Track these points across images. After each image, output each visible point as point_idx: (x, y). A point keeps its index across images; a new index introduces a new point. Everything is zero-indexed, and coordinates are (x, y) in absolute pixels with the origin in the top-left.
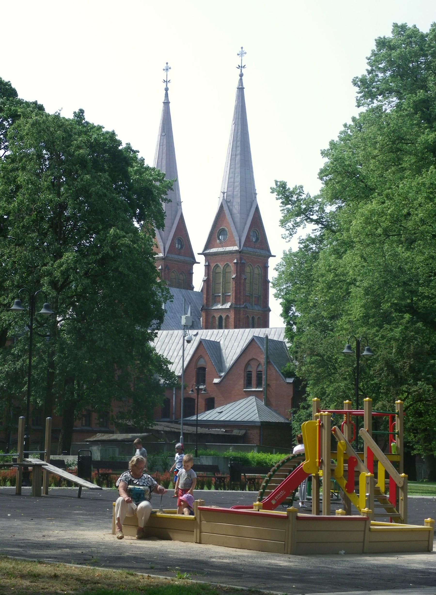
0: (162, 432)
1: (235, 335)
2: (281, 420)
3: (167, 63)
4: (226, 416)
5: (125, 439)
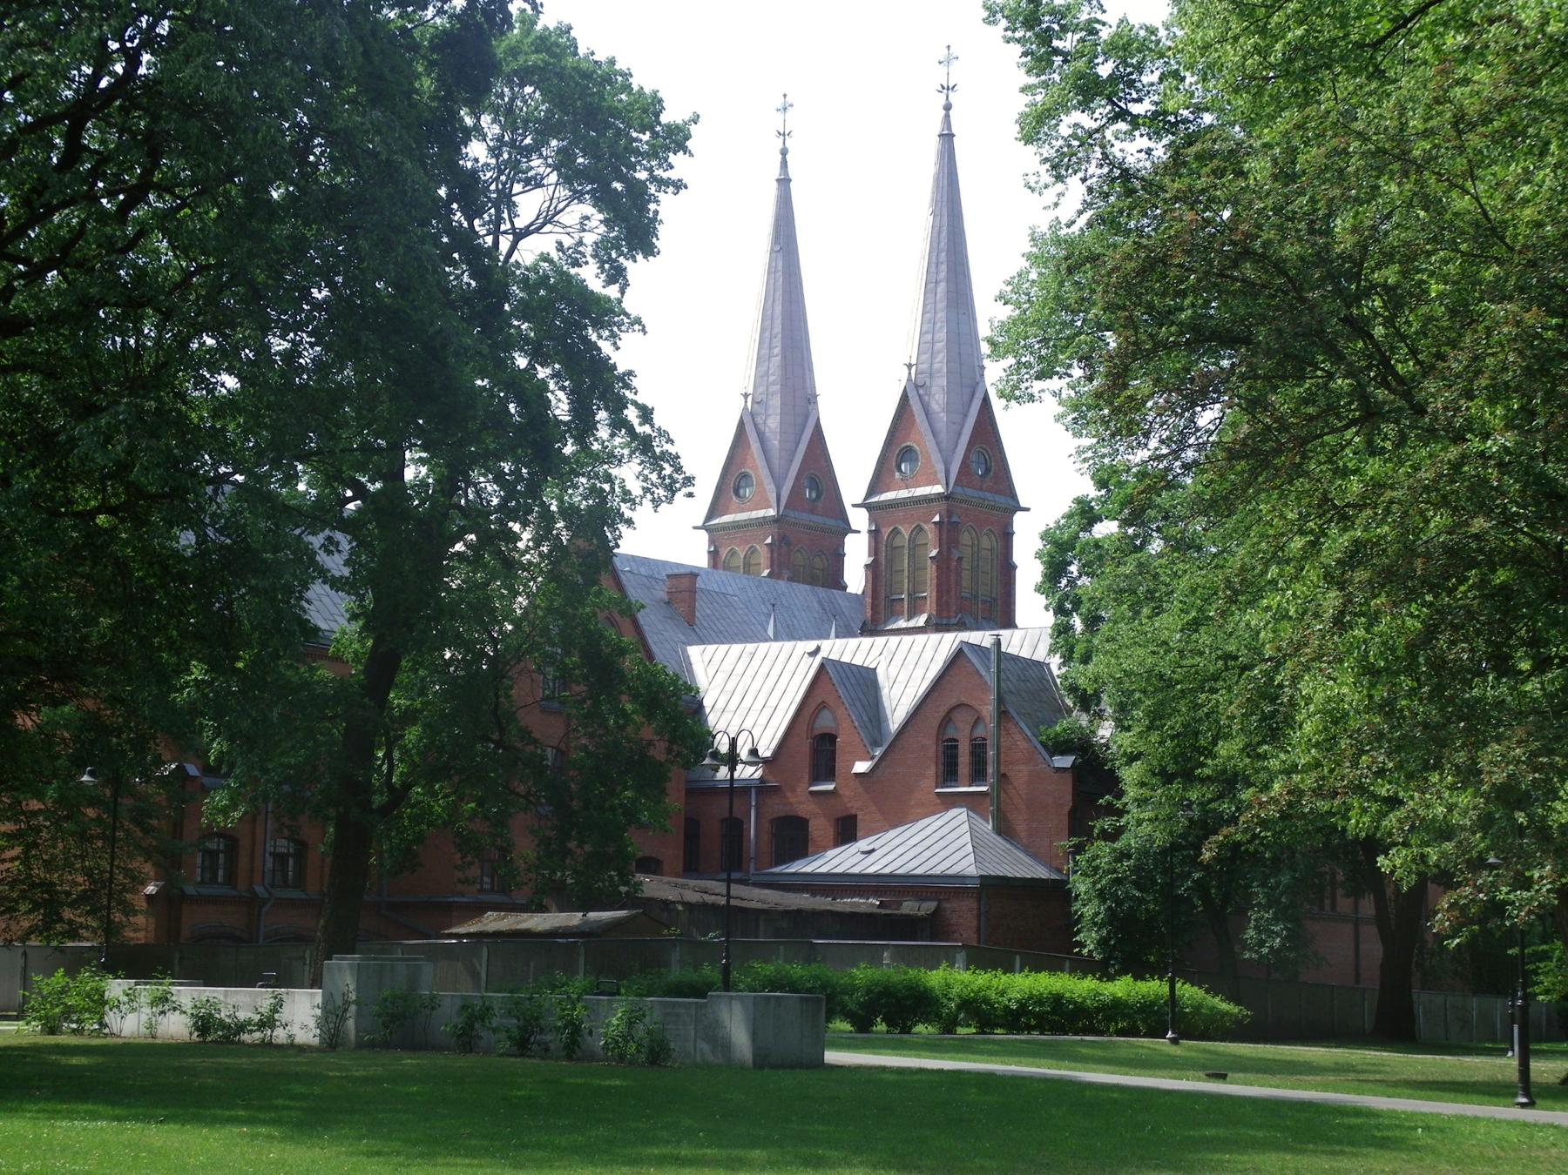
0: (680, 908)
1: (917, 649)
2: (1042, 872)
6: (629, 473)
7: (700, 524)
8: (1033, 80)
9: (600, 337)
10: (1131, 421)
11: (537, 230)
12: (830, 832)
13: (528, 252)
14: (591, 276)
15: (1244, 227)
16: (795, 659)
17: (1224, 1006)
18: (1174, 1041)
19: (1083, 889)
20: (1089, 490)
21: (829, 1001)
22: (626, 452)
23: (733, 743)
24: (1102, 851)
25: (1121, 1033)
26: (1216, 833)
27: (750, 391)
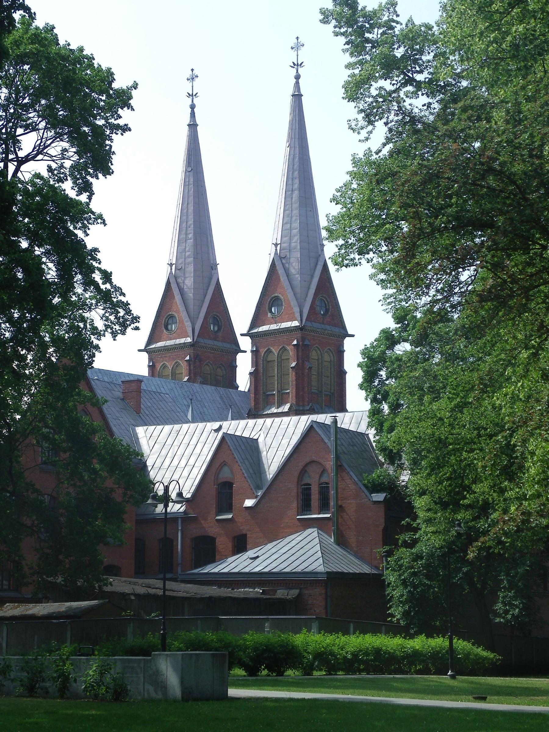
0: (133, 598)
1: (284, 426)
2: (366, 569)
3: (192, 70)
4: (265, 564)
5: (54, 613)
6: (96, 316)
7: (143, 348)
8: (354, 60)
9: (75, 228)
10: (418, 279)
11: (33, 159)
12: (230, 545)
13: (28, 171)
14: (68, 188)
15: (489, 153)
16: (205, 435)
17: (485, 654)
18: (453, 677)
19: (392, 579)
20: (391, 324)
21: (230, 656)
22: (94, 302)
23: (167, 488)
24: (404, 555)
25: (418, 672)
26: (477, 540)
27: (174, 262)
